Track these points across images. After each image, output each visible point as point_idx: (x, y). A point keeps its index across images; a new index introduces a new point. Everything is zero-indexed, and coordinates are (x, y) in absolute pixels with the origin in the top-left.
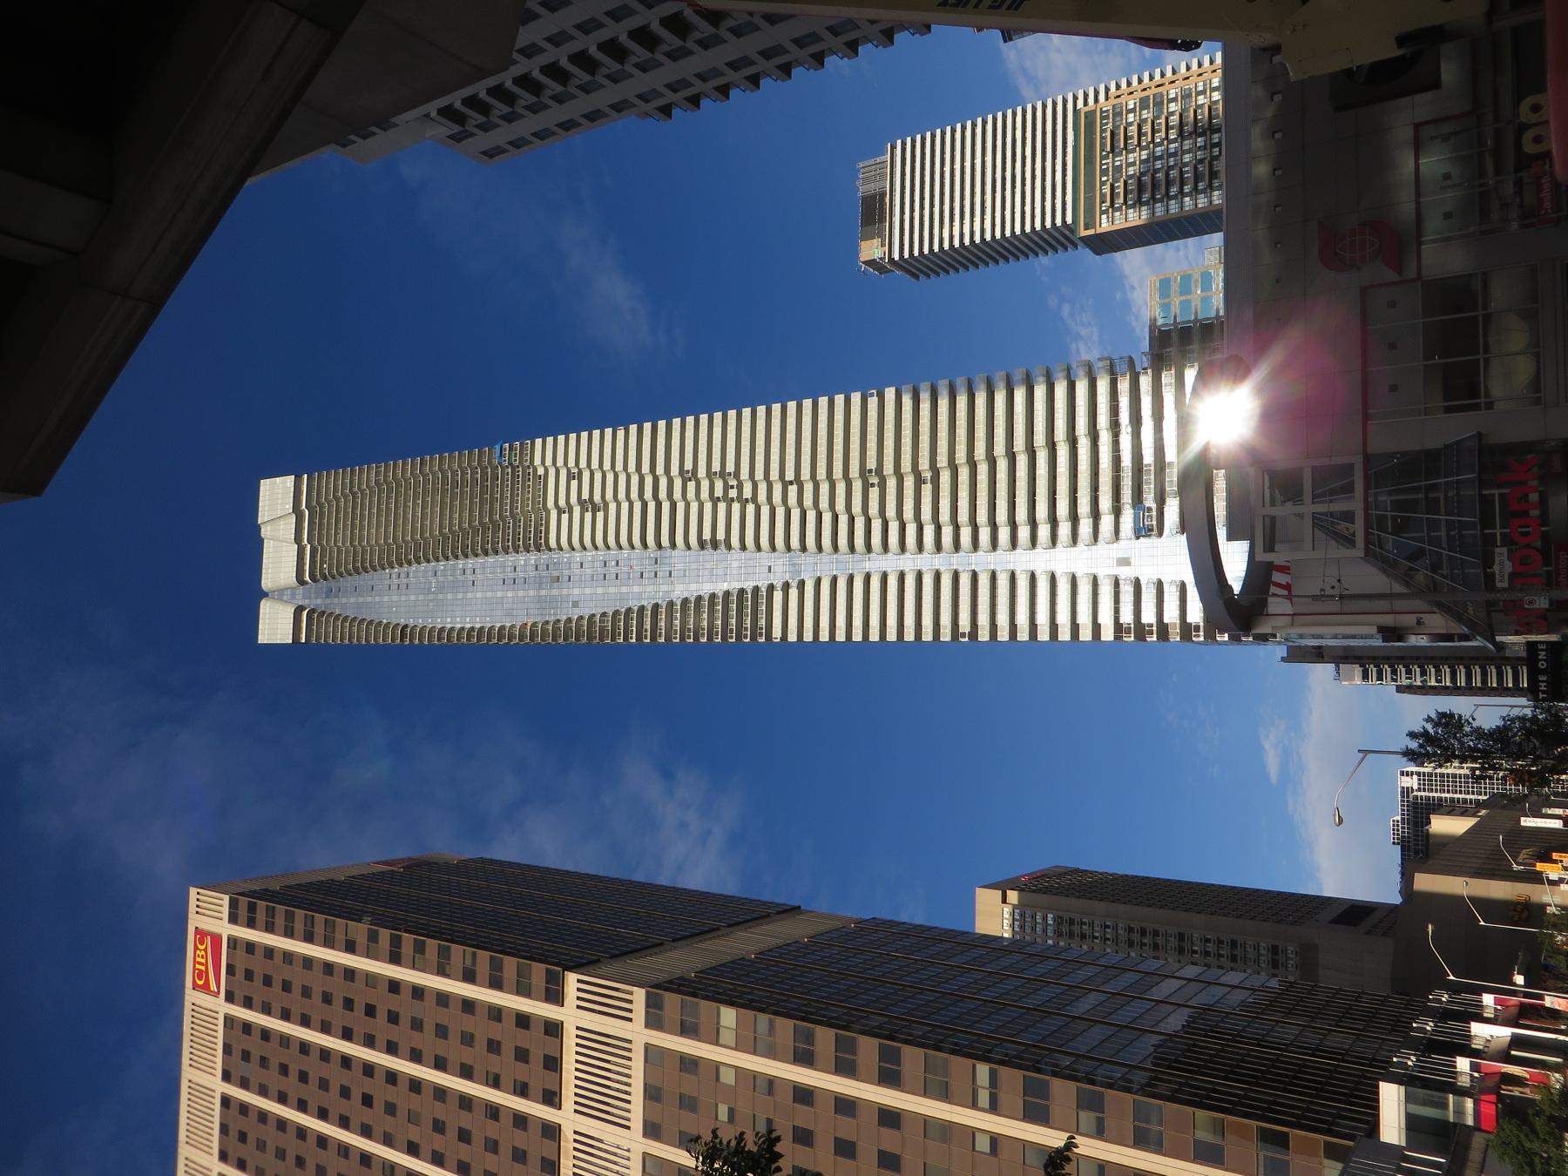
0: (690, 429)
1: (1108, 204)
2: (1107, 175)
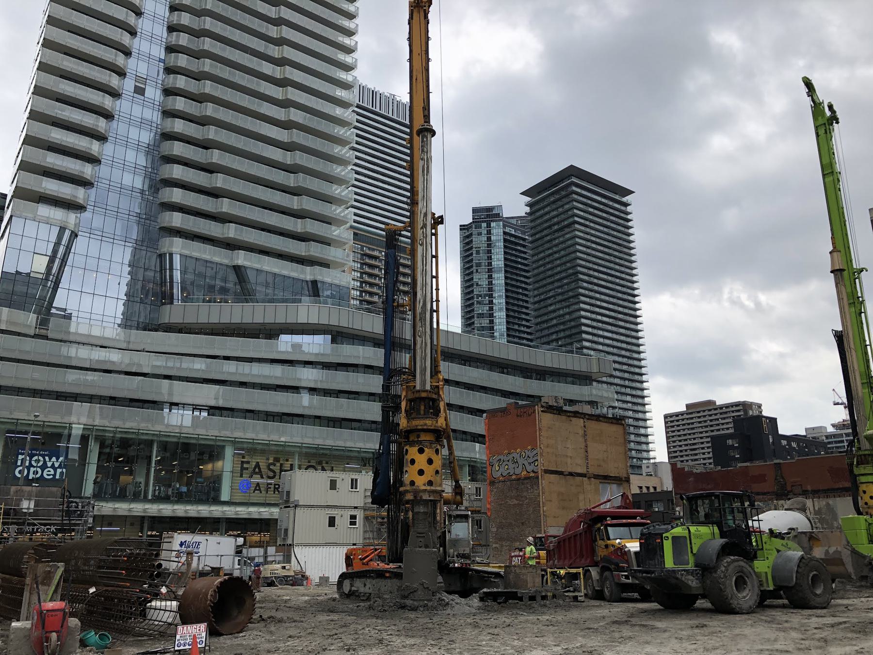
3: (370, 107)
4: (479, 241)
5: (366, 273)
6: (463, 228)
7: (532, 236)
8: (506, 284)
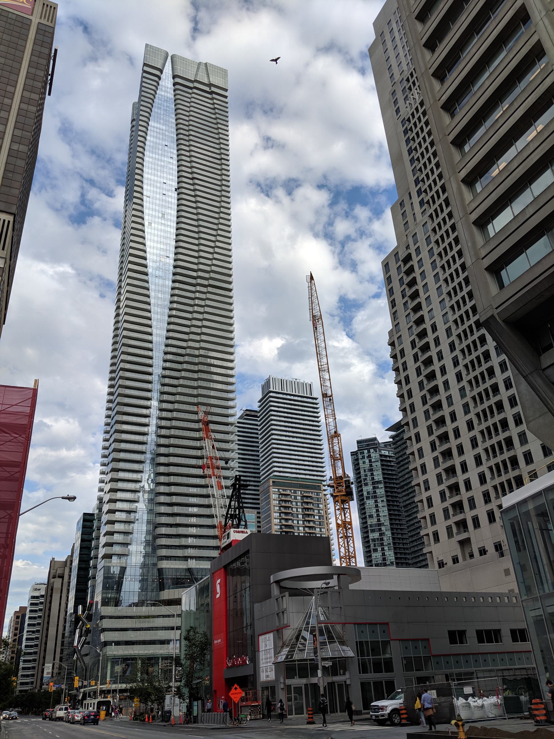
0: (205, 352)
1: (282, 492)
2: (294, 499)
3: (281, 391)
4: (364, 465)
5: (283, 513)
6: (353, 454)
7: (397, 464)
8: (390, 515)
